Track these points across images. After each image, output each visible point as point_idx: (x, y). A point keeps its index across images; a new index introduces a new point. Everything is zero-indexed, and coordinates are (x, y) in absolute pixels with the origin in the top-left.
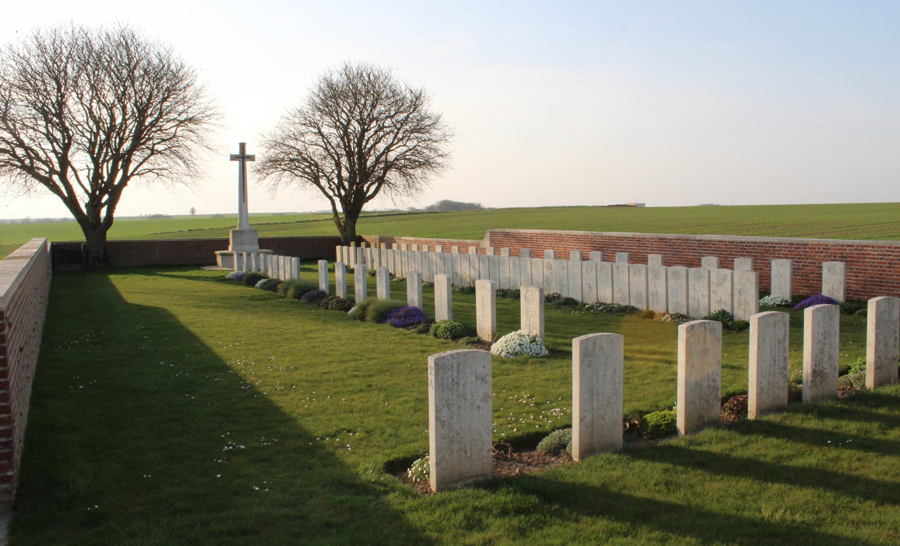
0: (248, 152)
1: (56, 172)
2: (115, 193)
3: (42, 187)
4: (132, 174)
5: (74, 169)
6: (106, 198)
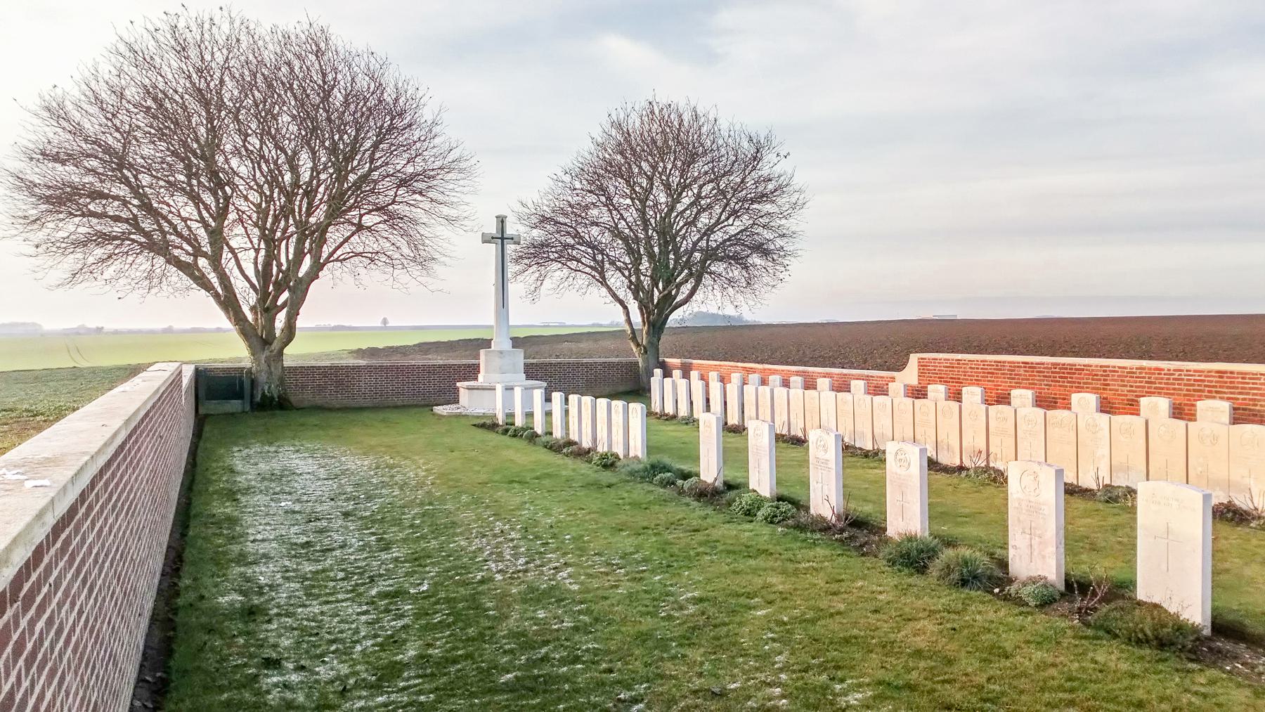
0: (510, 231)
1: (205, 255)
2: (300, 291)
4: (327, 261)
5: (232, 250)
6: (285, 295)
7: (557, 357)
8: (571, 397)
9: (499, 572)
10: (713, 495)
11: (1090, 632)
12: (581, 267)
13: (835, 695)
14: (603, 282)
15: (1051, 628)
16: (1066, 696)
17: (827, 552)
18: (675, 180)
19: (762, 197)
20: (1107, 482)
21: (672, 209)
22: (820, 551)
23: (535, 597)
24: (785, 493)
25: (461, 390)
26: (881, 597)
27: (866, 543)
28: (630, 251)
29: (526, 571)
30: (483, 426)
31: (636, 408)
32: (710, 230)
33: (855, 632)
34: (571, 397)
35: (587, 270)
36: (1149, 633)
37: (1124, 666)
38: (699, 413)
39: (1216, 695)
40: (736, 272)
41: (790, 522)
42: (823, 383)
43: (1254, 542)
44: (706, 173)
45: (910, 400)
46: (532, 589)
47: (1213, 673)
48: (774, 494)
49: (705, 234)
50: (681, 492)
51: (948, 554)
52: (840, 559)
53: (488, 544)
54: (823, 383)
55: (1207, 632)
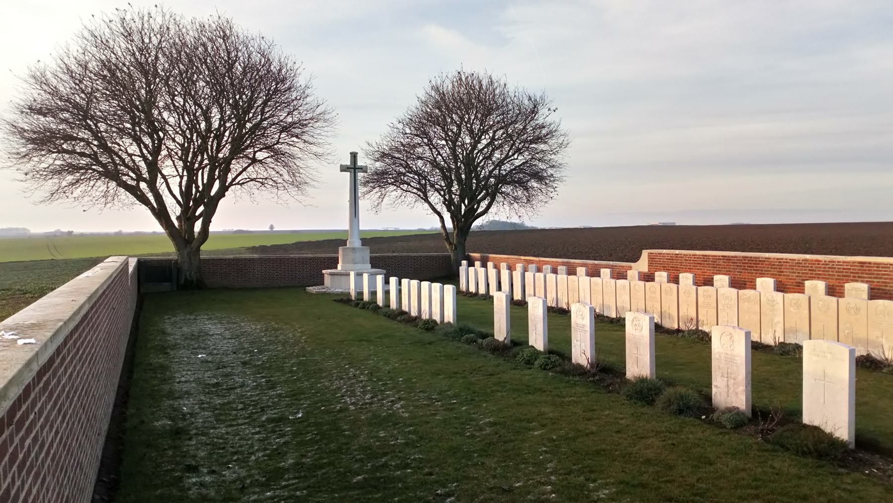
0: (360, 163)
3: (125, 196)
4: (231, 184)
5: (164, 177)
6: (201, 209)
7: (394, 252)
11: (769, 447)
13: (590, 491)
14: (426, 200)
16: (753, 492)
18: (476, 127)
19: (538, 139)
20: (781, 340)
22: (579, 389)
23: (378, 421)
24: (555, 348)
26: (622, 422)
28: (445, 178)
29: (371, 403)
30: (341, 301)
31: (449, 289)
32: (501, 163)
33: (604, 446)
35: (415, 191)
36: (811, 447)
37: (794, 471)
38: (493, 292)
40: (520, 193)
41: (558, 369)
42: (581, 271)
43: (885, 383)
44: (498, 122)
47: (856, 475)
49: (497, 165)
50: (481, 347)
51: (669, 392)
53: (345, 384)
54: (581, 271)
55: (852, 446)
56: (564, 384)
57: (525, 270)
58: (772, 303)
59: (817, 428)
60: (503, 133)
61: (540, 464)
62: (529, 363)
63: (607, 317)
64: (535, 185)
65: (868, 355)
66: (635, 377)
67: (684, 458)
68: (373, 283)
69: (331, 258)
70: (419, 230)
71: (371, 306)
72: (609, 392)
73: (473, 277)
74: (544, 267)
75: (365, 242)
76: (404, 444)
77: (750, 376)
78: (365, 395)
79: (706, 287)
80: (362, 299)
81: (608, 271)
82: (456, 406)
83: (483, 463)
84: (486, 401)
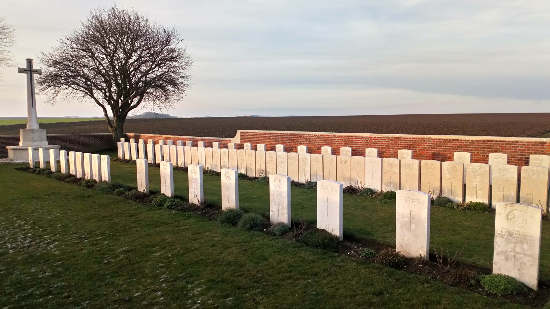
0: (35, 67)
7: (73, 133)
8: (70, 153)
9: (12, 249)
10: (143, 198)
11: (299, 244)
12: (79, 88)
13: (187, 291)
14: (92, 96)
15: (284, 244)
16: (288, 275)
17: (194, 220)
18: (128, 47)
19: (171, 59)
20: (309, 180)
21: (127, 61)
22: (191, 220)
23: (32, 260)
24: (179, 194)
25: (9, 151)
26: (216, 239)
27: (213, 214)
28: (106, 81)
29: (29, 247)
30: (21, 169)
31: (105, 158)
32: (147, 73)
33: (202, 257)
34: (70, 153)
35: (83, 89)
36: (320, 243)
37: (311, 258)
38: (158, 160)
39: (343, 266)
40: (160, 94)
41: (179, 208)
42: (201, 144)
43: (359, 201)
44: (143, 45)
45: (236, 150)
46: (31, 256)
47: (343, 256)
48: (173, 195)
49: (144, 75)
50: (127, 197)
51: (246, 216)
52: (200, 223)
53: (9, 233)
54: (201, 144)
55: (341, 239)
56: (182, 218)
57: (155, 143)
58: (304, 159)
59: (324, 231)
60: (148, 53)
61: (156, 276)
62: (160, 205)
63: (216, 172)
64: (171, 88)
65: (351, 186)
66: (226, 209)
67: (251, 259)
68: (46, 155)
69: (14, 138)
70: (94, 118)
71: (47, 172)
72: (211, 220)
73: (125, 149)
74: (177, 142)
75: (42, 126)
76: (50, 276)
77: (290, 203)
78: (25, 240)
79: (270, 152)
80: (39, 167)
81: (217, 143)
82: (100, 241)
83: (112, 283)
84: (124, 235)
